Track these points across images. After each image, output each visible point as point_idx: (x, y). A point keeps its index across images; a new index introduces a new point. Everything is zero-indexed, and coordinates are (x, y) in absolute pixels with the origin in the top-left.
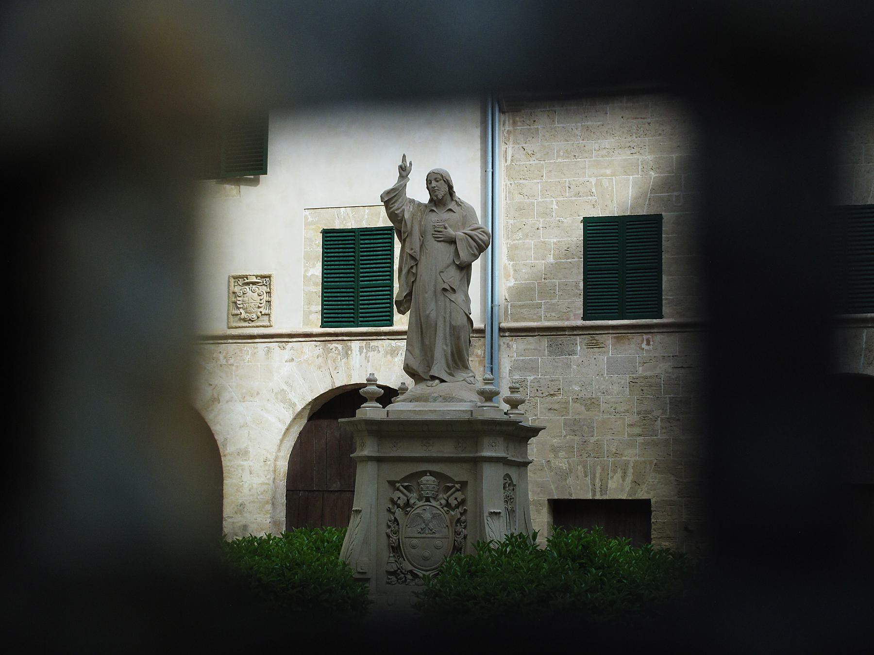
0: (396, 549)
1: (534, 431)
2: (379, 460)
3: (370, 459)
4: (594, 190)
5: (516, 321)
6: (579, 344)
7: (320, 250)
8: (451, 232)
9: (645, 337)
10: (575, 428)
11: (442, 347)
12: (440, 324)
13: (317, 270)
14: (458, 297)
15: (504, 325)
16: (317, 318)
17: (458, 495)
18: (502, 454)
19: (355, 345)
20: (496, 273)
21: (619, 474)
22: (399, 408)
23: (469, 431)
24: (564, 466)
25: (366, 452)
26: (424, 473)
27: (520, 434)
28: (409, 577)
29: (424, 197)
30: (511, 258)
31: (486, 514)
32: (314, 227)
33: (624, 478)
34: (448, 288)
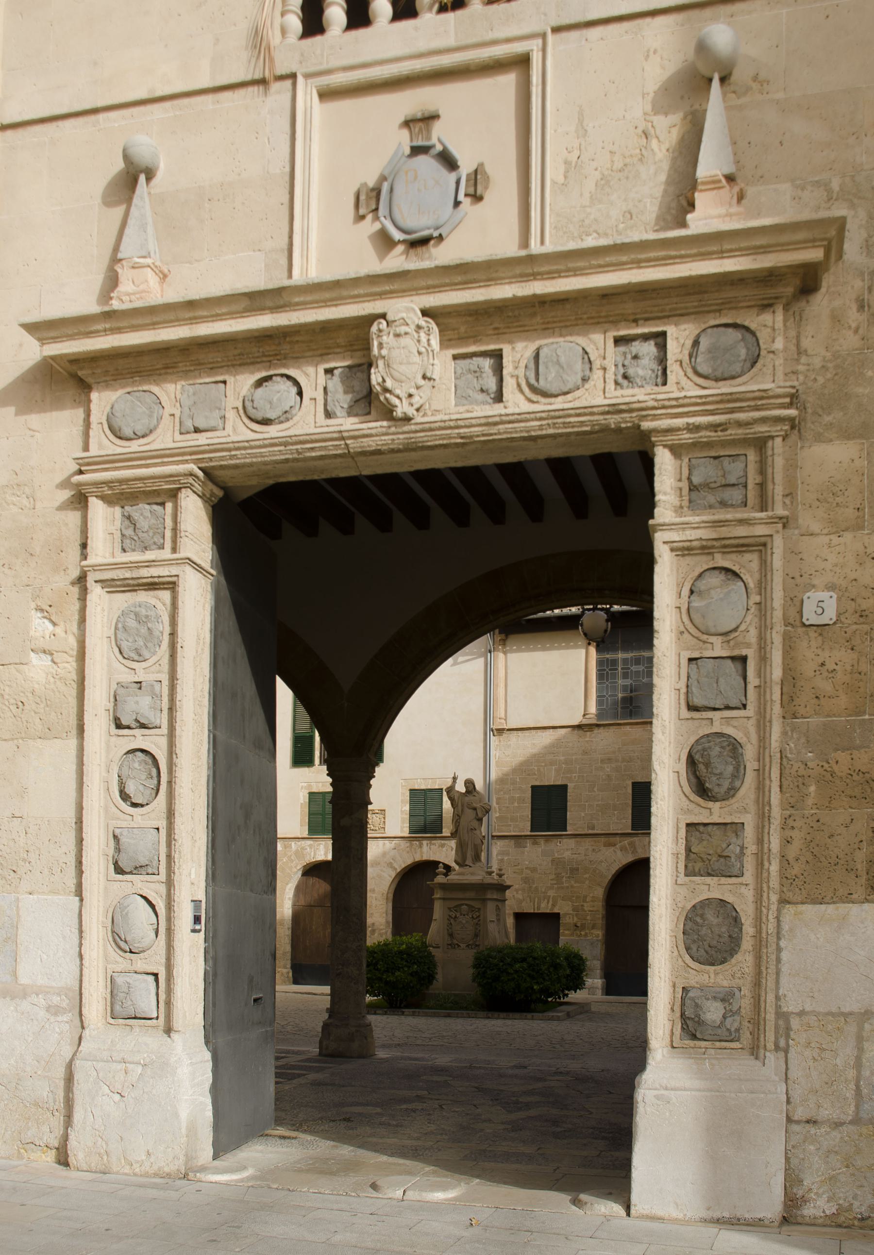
0: (451, 935)
1: (509, 887)
2: (444, 899)
3: (440, 898)
6: (529, 843)
8: (475, 805)
11: (470, 850)
12: (470, 843)
14: (477, 832)
15: (494, 834)
16: (407, 830)
17: (477, 914)
18: (495, 897)
19: (425, 842)
22: (453, 877)
23: (482, 888)
24: (521, 897)
25: (438, 896)
26: (463, 904)
27: (502, 888)
29: (463, 790)
33: (548, 903)
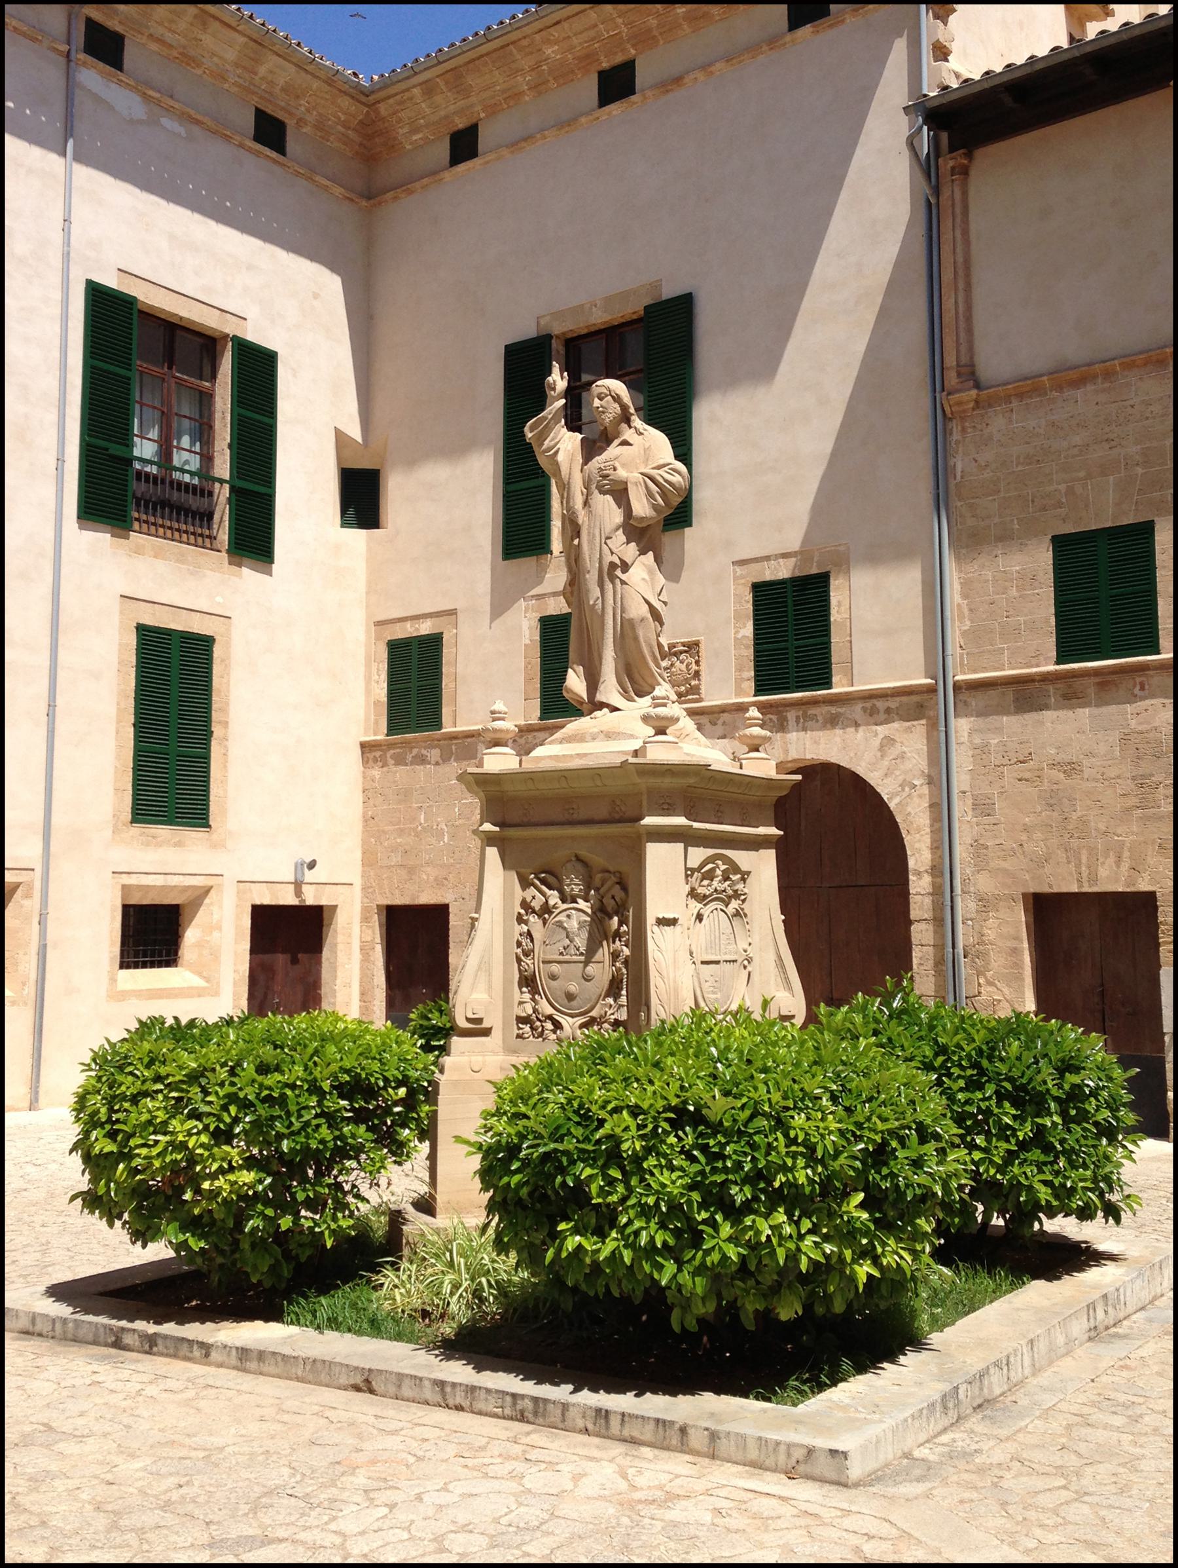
4: (1064, 500)
5: (975, 672)
7: (750, 606)
9: (1138, 680)
10: (1052, 801)
13: (748, 630)
16: (750, 686)
20: (948, 614)
21: (1111, 860)
28: (549, 1025)
30: (965, 596)
31: (650, 920)
32: (743, 581)
34: (618, 562)
